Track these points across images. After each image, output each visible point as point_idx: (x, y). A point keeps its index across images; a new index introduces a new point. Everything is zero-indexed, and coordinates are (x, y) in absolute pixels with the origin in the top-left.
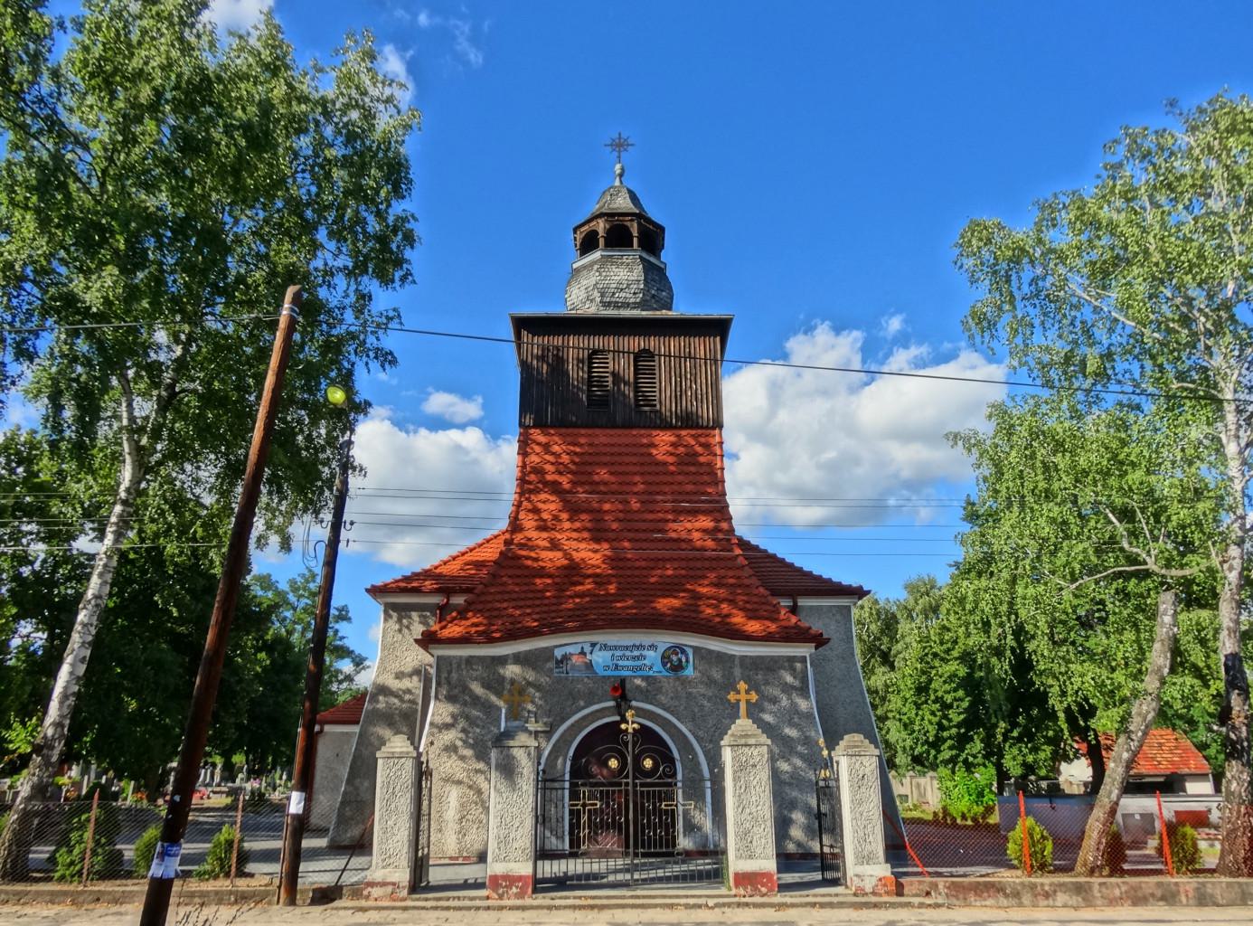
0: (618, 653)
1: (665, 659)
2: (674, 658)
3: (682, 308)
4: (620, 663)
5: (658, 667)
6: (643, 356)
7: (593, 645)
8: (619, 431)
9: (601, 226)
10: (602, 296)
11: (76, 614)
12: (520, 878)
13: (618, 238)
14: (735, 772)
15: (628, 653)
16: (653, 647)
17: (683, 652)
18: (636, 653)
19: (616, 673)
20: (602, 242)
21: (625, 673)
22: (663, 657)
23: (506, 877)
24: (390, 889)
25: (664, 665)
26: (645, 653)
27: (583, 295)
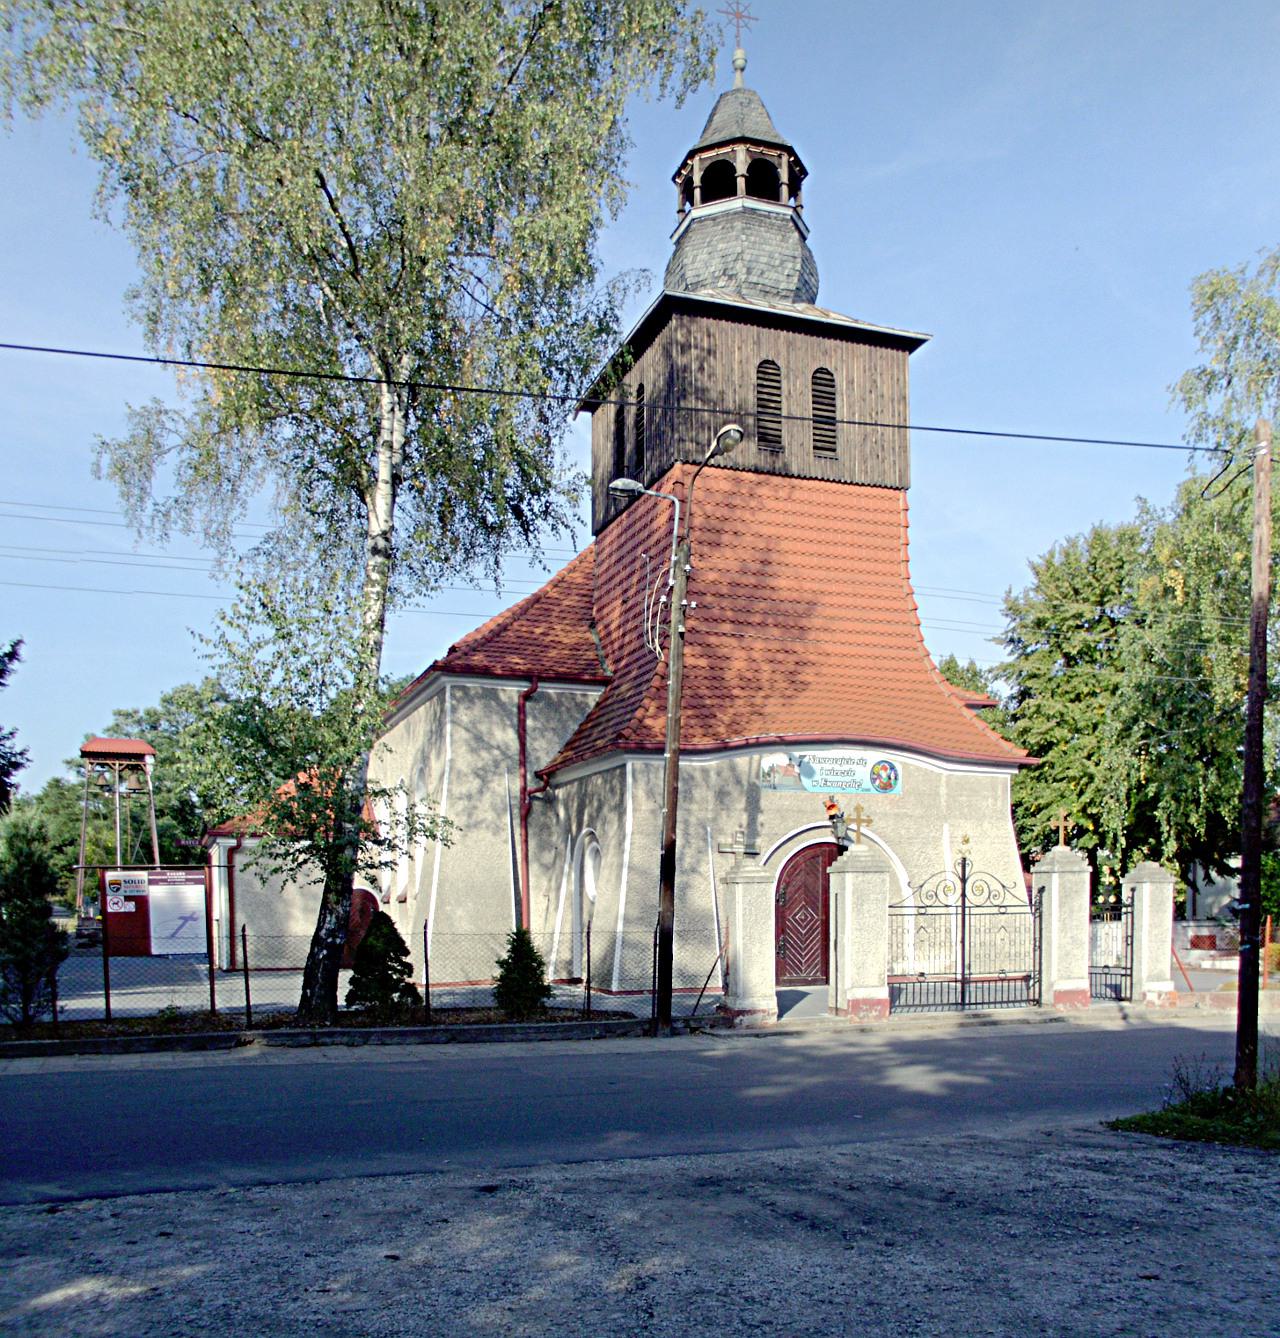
1: (874, 777)
2: (884, 774)
3: (829, 308)
4: (830, 778)
5: (867, 784)
9: (741, 161)
10: (749, 272)
11: (1249, 709)
12: (879, 1002)
13: (719, 181)
14: (1061, 898)
15: (837, 767)
16: (862, 762)
17: (893, 768)
18: (846, 767)
20: (741, 183)
22: (873, 773)
23: (866, 1001)
25: (873, 780)
26: (854, 767)
27: (716, 265)
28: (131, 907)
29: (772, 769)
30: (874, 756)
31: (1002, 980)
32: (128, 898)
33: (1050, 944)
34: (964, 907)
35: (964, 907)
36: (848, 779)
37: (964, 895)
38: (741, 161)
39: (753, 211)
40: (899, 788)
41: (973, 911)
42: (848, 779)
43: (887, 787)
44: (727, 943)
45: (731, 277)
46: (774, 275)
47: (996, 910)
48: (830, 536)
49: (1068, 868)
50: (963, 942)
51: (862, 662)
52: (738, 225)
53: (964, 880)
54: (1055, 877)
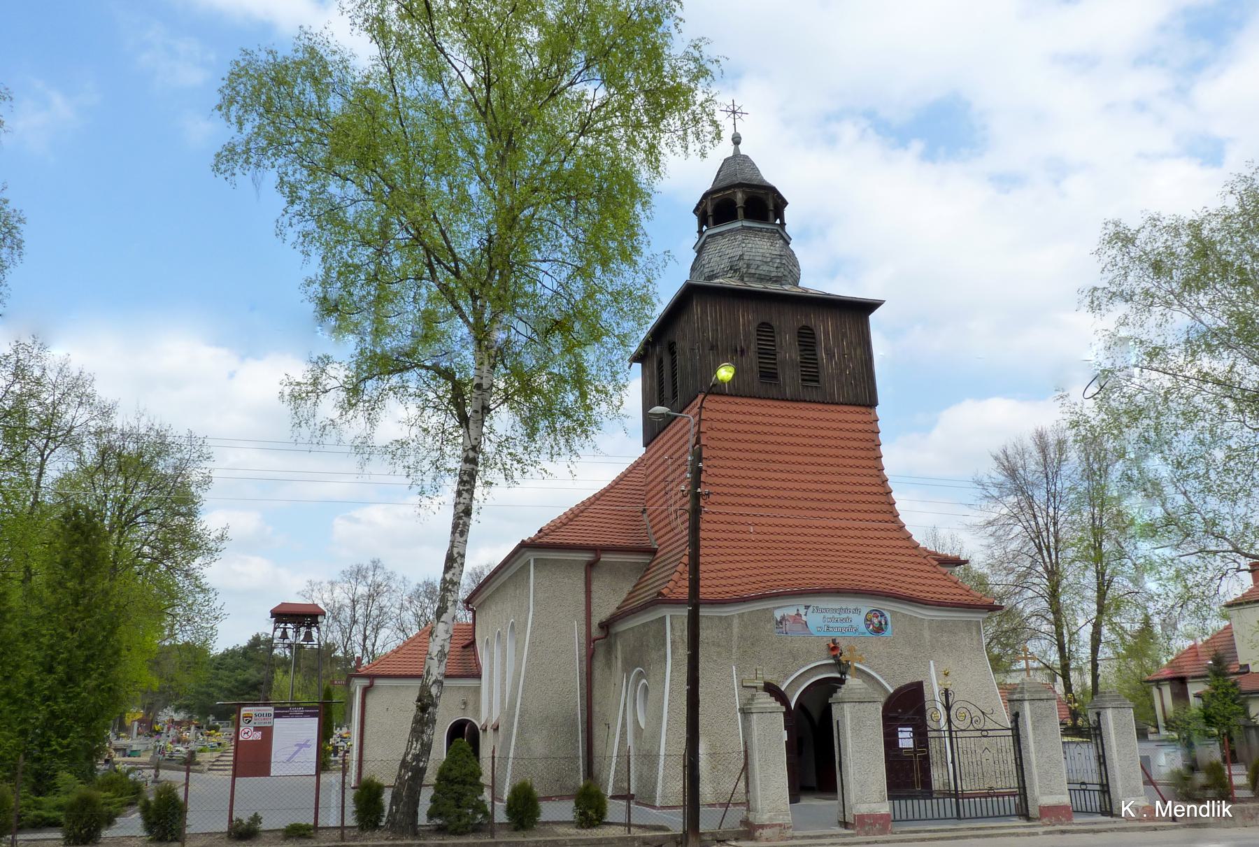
0: (829, 615)
1: (868, 621)
2: (876, 621)
4: (831, 625)
5: (862, 627)
6: (765, 328)
7: (807, 607)
8: (789, 404)
15: (837, 616)
16: (857, 610)
17: (882, 615)
19: (829, 634)
20: (740, 212)
21: (834, 635)
22: (866, 620)
23: (869, 816)
24: (776, 830)
26: (851, 615)
28: (258, 736)
29: (783, 618)
30: (866, 606)
32: (256, 729)
33: (1030, 763)
36: (846, 625)
39: (750, 228)
40: (888, 632)
41: (960, 734)
42: (846, 625)
43: (879, 630)
46: (765, 268)
47: (978, 734)
52: (739, 237)
54: (1027, 704)
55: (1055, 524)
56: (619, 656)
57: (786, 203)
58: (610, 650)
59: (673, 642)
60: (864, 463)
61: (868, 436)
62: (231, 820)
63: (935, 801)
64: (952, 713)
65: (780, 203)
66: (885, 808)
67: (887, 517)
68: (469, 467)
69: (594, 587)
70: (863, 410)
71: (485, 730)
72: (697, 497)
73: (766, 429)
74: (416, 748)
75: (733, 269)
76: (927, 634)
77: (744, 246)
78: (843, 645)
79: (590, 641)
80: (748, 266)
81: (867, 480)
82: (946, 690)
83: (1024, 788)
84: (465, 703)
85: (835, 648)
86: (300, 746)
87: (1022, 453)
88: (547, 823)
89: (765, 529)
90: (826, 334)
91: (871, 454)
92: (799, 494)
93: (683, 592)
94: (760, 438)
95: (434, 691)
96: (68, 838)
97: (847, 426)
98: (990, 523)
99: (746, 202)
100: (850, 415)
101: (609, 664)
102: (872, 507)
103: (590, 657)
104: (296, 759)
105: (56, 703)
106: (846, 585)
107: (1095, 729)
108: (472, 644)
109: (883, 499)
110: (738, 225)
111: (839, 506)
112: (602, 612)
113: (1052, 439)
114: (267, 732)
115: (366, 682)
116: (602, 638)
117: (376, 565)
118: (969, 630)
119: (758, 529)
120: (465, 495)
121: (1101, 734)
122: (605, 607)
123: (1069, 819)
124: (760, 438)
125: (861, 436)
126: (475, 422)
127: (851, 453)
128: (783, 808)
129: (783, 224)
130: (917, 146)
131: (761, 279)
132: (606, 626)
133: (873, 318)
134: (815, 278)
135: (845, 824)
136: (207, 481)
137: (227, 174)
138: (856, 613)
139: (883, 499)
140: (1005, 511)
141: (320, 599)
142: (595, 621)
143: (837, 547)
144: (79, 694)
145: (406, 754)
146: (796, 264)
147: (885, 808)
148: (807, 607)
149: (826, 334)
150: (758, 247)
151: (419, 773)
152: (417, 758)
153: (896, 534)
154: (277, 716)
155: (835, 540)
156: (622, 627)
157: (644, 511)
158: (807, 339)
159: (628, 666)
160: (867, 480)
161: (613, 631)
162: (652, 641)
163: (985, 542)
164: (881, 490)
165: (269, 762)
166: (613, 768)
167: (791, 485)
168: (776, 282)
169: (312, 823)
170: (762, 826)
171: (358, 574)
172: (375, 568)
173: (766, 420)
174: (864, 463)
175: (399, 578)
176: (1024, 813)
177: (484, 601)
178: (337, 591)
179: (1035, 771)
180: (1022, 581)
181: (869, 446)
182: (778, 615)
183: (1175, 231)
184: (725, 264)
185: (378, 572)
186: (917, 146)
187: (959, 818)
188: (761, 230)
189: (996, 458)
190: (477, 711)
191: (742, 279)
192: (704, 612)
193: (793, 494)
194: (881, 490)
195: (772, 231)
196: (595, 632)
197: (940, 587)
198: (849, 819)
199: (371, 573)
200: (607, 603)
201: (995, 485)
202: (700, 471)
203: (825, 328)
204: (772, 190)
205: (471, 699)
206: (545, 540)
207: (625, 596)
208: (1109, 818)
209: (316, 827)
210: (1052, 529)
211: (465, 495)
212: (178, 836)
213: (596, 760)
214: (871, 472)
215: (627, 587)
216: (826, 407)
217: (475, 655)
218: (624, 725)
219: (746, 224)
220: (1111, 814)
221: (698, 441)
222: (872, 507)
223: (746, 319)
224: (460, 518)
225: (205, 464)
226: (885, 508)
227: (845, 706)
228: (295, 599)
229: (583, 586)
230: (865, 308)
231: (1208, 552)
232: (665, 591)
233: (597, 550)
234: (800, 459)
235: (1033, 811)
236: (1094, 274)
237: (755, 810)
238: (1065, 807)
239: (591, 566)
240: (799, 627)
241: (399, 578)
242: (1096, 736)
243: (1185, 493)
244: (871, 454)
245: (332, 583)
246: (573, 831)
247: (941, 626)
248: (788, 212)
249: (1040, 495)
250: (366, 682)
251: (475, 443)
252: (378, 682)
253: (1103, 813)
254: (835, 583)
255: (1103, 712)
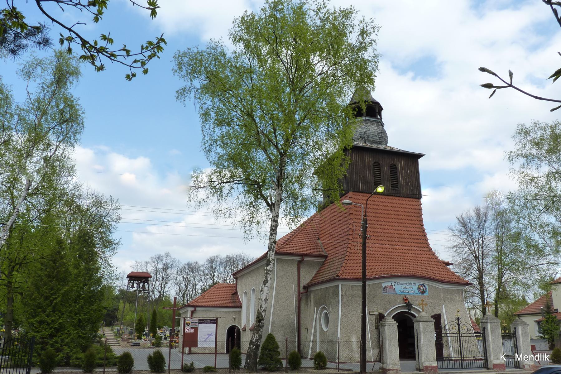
0: (403, 286)
1: (419, 289)
2: (422, 288)
5: (417, 291)
6: (377, 165)
7: (395, 282)
12: (434, 367)
16: (415, 284)
17: (425, 286)
18: (409, 286)
21: (406, 294)
23: (430, 367)
24: (395, 371)
26: (412, 286)
28: (192, 331)
29: (386, 287)
30: (418, 282)
31: (474, 360)
32: (192, 328)
33: (489, 347)
34: (459, 334)
35: (459, 334)
37: (459, 330)
38: (364, 107)
39: (369, 120)
41: (463, 335)
42: (410, 290)
43: (423, 292)
44: (382, 345)
45: (362, 138)
46: (375, 138)
47: (470, 335)
48: (398, 213)
49: (493, 321)
50: (460, 346)
51: (411, 252)
52: (364, 124)
53: (459, 324)
54: (489, 324)
55: (482, 248)
56: (312, 299)
57: (382, 109)
58: (308, 297)
59: (342, 296)
60: (416, 222)
61: (417, 211)
62: (182, 365)
63: (444, 362)
64: (460, 326)
65: (381, 109)
66: (435, 364)
67: (425, 245)
68: (275, 223)
69: (301, 271)
70: (416, 200)
71: (244, 330)
72: (365, 238)
73: (377, 207)
74: (257, 336)
75: (362, 137)
76: (442, 294)
77: (361, 128)
78: (409, 298)
79: (299, 294)
80: (368, 137)
81: (417, 230)
82: (458, 319)
83: (487, 357)
84: (234, 319)
85: (406, 299)
86: (209, 335)
87: (469, 217)
88: (305, 368)
89: (376, 249)
90: (401, 167)
91: (419, 219)
92: (390, 235)
93: (360, 275)
94: (374, 211)
95: (263, 314)
96: (120, 371)
97: (409, 207)
98: (455, 247)
99: (367, 109)
100: (410, 202)
101: (307, 304)
102: (419, 241)
103: (299, 301)
104: (208, 340)
105: (80, 316)
106: (411, 273)
107: (513, 334)
108: (236, 293)
109: (423, 238)
110: (364, 118)
111: (406, 240)
112: (305, 281)
113: (482, 211)
114: (196, 329)
115: (193, 309)
116: (305, 293)
117: (167, 255)
118: (458, 293)
119: (374, 249)
120: (274, 235)
121: (516, 336)
122: (306, 279)
123: (504, 369)
124: (374, 211)
125: (414, 211)
126: (277, 205)
127: (411, 218)
128: (397, 363)
129: (381, 118)
130: (411, 74)
131: (373, 142)
132: (306, 288)
133: (420, 161)
134: (395, 142)
135: (419, 370)
136: (118, 219)
137: (182, 100)
138: (414, 286)
139: (423, 238)
140: (461, 241)
141: (150, 269)
142: (302, 286)
143: (405, 258)
144: (89, 312)
145: (252, 339)
146: (387, 136)
147: (435, 364)
148: (395, 282)
149: (401, 167)
150: (373, 129)
151: (258, 346)
152: (257, 341)
153: (429, 253)
154: (200, 323)
155: (405, 255)
156: (313, 289)
157: (319, 239)
158: (393, 169)
159: (317, 305)
160: (417, 230)
161: (309, 290)
162: (331, 294)
163: (451, 254)
164: (422, 234)
165: (197, 341)
166: (311, 346)
167: (387, 231)
168: (379, 144)
169: (214, 366)
170: (390, 370)
171: (159, 258)
172: (167, 256)
173: (376, 203)
174: (416, 222)
175: (177, 261)
176: (486, 367)
177: (243, 275)
178: (149, 265)
179: (491, 350)
180: (468, 270)
181: (417, 215)
182: (384, 285)
183: (544, 129)
184: (358, 135)
185: (168, 258)
186: (411, 74)
187: (462, 368)
188: (373, 121)
189: (458, 219)
190: (240, 322)
191: (365, 142)
192: (368, 283)
193: (387, 235)
194: (422, 234)
195: (378, 122)
196: (302, 290)
197: (437, 274)
198: (421, 367)
199: (165, 258)
200: (307, 277)
201: (458, 230)
202: (366, 227)
203: (401, 165)
204: (378, 104)
205: (237, 317)
206: (281, 251)
207: (313, 275)
208: (518, 369)
209: (215, 368)
210: (481, 249)
211: (274, 235)
212: (129, 370)
213: (302, 343)
214: (418, 226)
215: (315, 272)
216: (401, 198)
217: (238, 297)
218: (315, 329)
219: (367, 118)
220: (519, 367)
221: (365, 216)
222: (419, 241)
223: (369, 160)
224: (272, 245)
225: (119, 211)
226: (424, 241)
227: (421, 323)
228: (140, 270)
229: (296, 270)
230: (414, 158)
231: (551, 263)
232: (339, 274)
233: (303, 255)
234: (390, 220)
235: (490, 366)
236: (512, 146)
237: (386, 363)
238: (503, 365)
239: (300, 263)
240: (392, 290)
241: (177, 261)
242: (514, 337)
243: (544, 239)
244: (419, 219)
245: (146, 263)
246: (314, 371)
247: (447, 292)
248: (383, 112)
249: (476, 235)
250: (193, 309)
251: (277, 214)
252: (198, 309)
253: (515, 368)
254: (406, 273)
255: (517, 327)
